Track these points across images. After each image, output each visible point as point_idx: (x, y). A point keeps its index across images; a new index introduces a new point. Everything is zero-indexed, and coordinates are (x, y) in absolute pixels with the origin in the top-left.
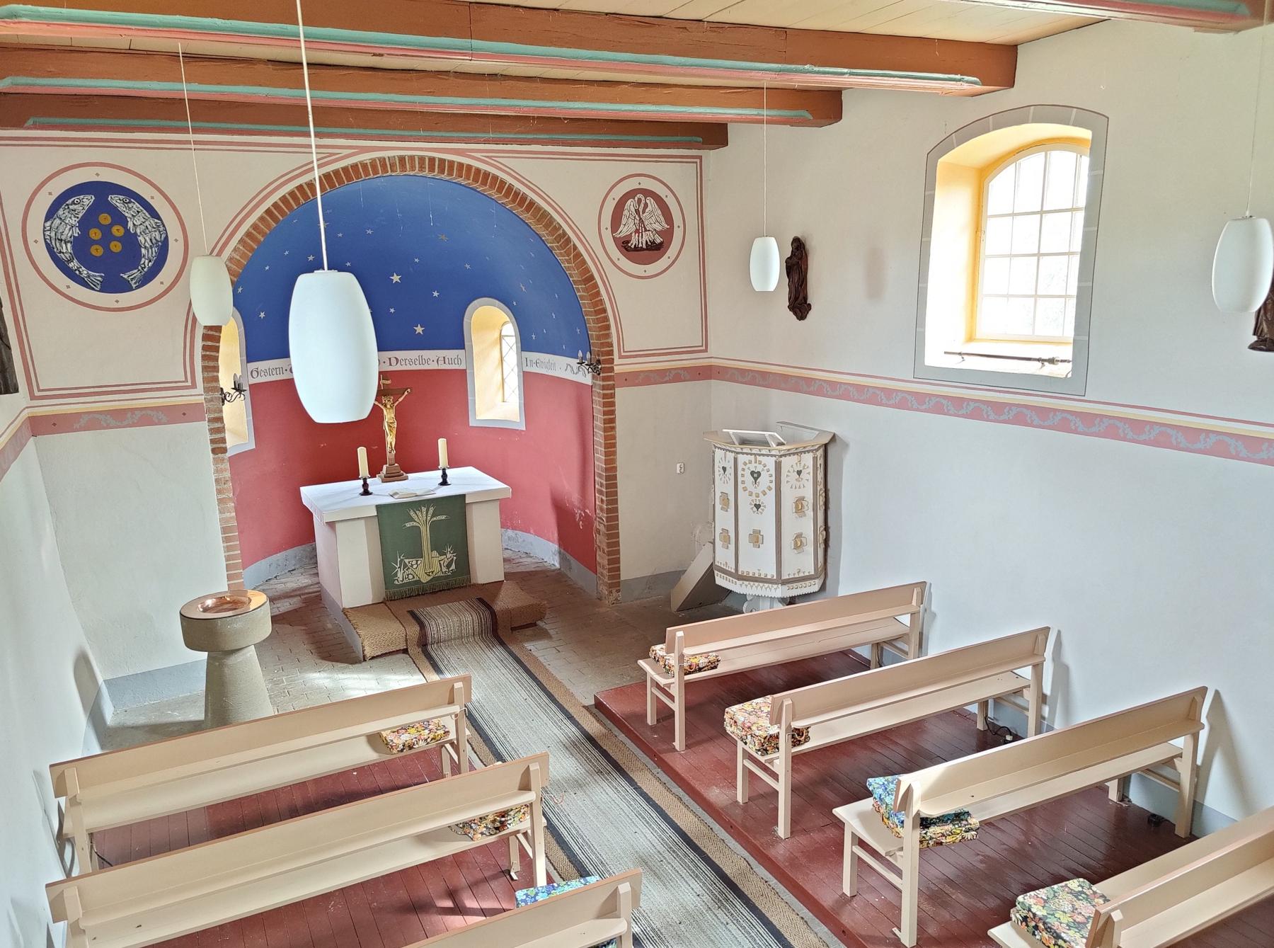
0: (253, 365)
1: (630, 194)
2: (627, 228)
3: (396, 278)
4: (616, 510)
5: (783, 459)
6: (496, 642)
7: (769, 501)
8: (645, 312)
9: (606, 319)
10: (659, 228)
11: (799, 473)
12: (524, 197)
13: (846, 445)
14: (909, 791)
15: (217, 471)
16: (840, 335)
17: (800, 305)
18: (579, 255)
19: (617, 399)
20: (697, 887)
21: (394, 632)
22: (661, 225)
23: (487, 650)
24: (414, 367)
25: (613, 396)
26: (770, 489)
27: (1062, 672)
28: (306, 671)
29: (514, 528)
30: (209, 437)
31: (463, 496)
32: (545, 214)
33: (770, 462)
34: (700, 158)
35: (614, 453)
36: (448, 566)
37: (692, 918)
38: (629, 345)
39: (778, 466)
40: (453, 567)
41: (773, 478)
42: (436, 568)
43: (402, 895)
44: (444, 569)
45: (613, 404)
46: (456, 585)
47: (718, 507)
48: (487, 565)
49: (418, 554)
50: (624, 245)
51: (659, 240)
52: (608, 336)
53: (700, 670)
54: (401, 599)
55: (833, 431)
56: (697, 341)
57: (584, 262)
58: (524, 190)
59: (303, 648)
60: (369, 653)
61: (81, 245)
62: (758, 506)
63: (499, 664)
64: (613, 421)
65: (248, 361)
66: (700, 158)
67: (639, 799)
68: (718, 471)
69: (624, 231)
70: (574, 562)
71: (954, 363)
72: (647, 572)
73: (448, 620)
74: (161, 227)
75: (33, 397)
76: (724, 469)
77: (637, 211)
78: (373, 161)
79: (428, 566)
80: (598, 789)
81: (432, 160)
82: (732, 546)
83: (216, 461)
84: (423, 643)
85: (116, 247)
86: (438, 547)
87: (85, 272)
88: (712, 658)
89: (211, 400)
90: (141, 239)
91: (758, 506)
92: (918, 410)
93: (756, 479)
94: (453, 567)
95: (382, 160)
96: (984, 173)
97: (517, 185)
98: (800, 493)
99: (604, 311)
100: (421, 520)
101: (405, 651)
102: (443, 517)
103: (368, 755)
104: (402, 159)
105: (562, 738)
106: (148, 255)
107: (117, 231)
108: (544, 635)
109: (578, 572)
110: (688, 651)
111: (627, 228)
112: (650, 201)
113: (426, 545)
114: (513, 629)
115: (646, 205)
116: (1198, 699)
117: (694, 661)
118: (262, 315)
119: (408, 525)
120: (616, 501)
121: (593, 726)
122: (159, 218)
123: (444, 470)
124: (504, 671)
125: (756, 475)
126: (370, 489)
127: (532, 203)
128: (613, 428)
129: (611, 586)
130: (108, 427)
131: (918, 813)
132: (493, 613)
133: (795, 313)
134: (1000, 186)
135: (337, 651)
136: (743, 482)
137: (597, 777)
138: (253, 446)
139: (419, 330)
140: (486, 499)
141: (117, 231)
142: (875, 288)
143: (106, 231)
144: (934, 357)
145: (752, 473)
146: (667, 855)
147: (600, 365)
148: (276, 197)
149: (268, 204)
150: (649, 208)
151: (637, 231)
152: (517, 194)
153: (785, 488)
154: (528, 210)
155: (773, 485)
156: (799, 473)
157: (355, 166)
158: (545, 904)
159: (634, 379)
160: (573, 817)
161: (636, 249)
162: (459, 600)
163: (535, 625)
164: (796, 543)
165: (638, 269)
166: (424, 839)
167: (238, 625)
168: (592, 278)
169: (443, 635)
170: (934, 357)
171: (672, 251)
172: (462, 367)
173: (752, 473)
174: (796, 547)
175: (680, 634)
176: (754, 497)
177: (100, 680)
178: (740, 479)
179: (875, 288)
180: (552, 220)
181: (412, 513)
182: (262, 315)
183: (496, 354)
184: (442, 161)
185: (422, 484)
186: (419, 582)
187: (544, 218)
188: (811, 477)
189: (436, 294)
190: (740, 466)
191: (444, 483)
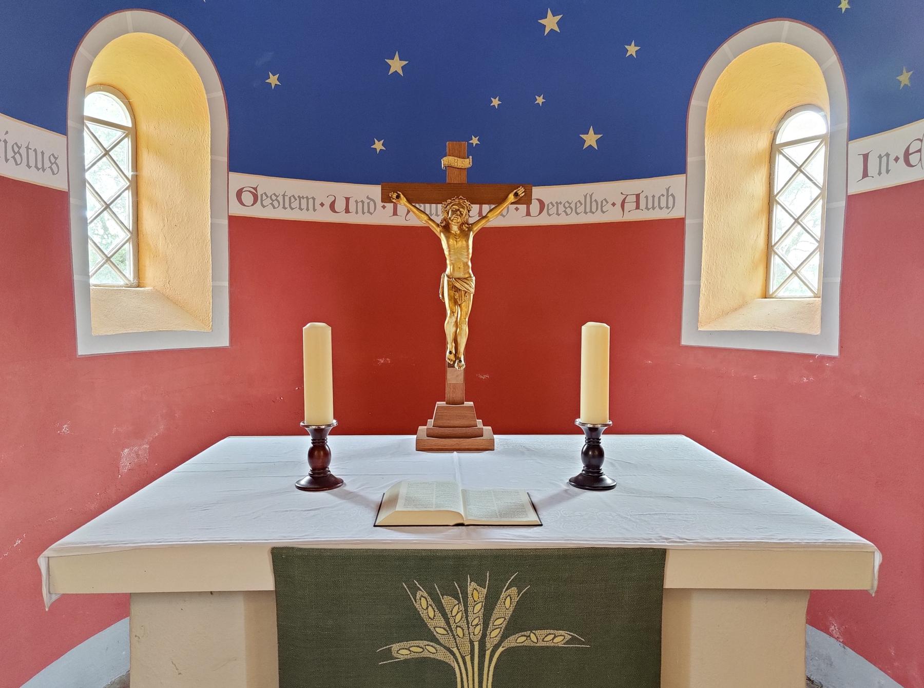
31: (653, 560)
102: (559, 638)
119: (403, 651)
123: (593, 434)
126: (334, 469)
138: (223, 341)
172: (676, 213)
183: (757, 185)
191: (591, 479)
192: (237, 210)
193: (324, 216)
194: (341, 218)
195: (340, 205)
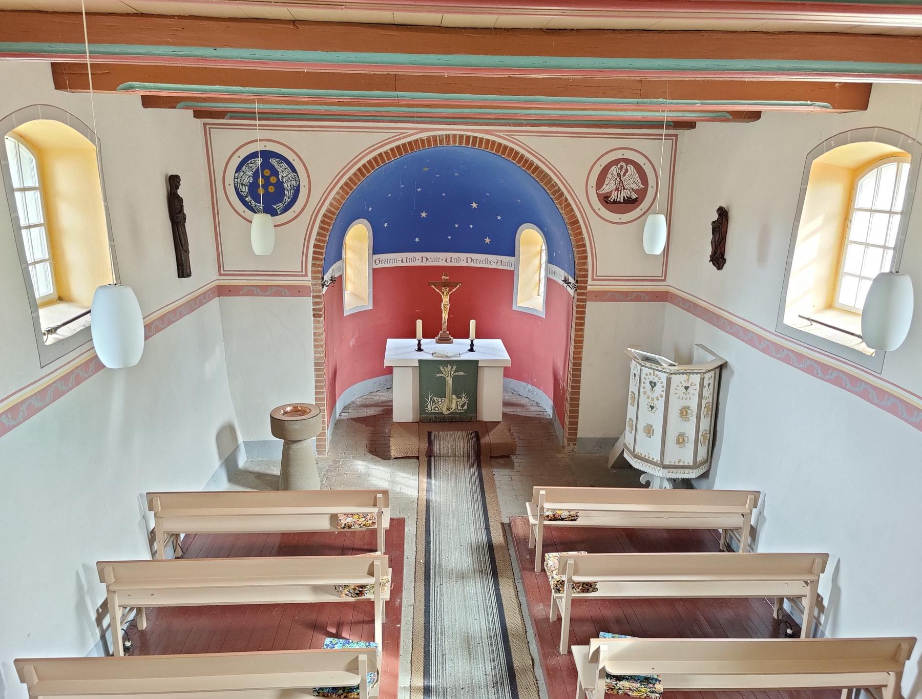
0: (376, 257)
1: (615, 162)
2: (609, 186)
5: (673, 376)
6: (475, 464)
9: (585, 252)
10: (635, 187)
11: (687, 388)
12: (532, 164)
13: (733, 372)
14: (597, 651)
15: (315, 328)
16: (735, 290)
17: (718, 259)
18: (569, 205)
19: (587, 310)
20: (489, 667)
21: (413, 444)
23: (466, 464)
25: (584, 307)
26: (662, 396)
27: (836, 591)
28: (354, 457)
29: (532, 384)
30: (312, 307)
31: (477, 361)
32: (546, 175)
33: (664, 377)
34: (676, 136)
35: (581, 347)
36: (463, 406)
37: (472, 688)
39: (669, 380)
40: (466, 407)
42: (454, 406)
43: (313, 617)
45: (584, 313)
46: (467, 420)
47: (630, 401)
48: (491, 408)
49: (443, 395)
50: (605, 200)
51: (634, 196)
52: (585, 264)
53: (562, 519)
54: (429, 424)
55: (727, 359)
56: (658, 272)
57: (572, 210)
58: (531, 158)
59: (364, 442)
60: (393, 454)
61: (253, 187)
62: (652, 407)
63: (467, 480)
64: (583, 324)
65: (374, 254)
66: (676, 136)
67: (493, 597)
68: (632, 375)
69: (606, 189)
70: (557, 419)
71: (803, 326)
72: (598, 435)
73: (452, 442)
74: (297, 179)
75: (220, 274)
77: (619, 175)
78: (428, 138)
80: (472, 583)
81: (468, 137)
82: (633, 432)
83: (315, 322)
84: (429, 456)
85: (271, 189)
86: (457, 393)
87: (254, 203)
88: (573, 513)
89: (315, 285)
91: (652, 407)
92: (774, 357)
93: (653, 387)
94: (466, 407)
95: (435, 137)
96: (857, 172)
97: (527, 155)
98: (686, 403)
99: (584, 245)
100: (448, 373)
101: (417, 458)
103: (323, 525)
104: (448, 136)
105: (474, 541)
106: (288, 194)
107: (273, 180)
108: (510, 465)
109: (557, 424)
110: (547, 506)
111: (609, 186)
112: (631, 169)
113: (449, 390)
114: (491, 457)
115: (627, 171)
116: (905, 647)
117: (559, 512)
118: (386, 225)
120: (579, 382)
121: (498, 537)
124: (468, 486)
125: (653, 384)
127: (537, 168)
128: (582, 330)
129: (569, 440)
130: (258, 295)
131: (604, 668)
132: (479, 445)
134: (867, 184)
135: (379, 450)
136: (644, 388)
137: (477, 575)
138: (371, 307)
139: (487, 240)
140: (494, 365)
142: (762, 258)
144: (791, 319)
145: (651, 382)
146: (485, 640)
147: (580, 282)
148: (364, 161)
149: (360, 165)
150: (629, 172)
151: (617, 189)
152: (526, 161)
153: (672, 398)
154: (533, 172)
155: (664, 394)
157: (416, 141)
158: (338, 651)
159: (601, 296)
160: (445, 598)
161: (615, 202)
163: (508, 457)
165: (615, 217)
166: (316, 589)
167: (297, 427)
168: (577, 221)
169: (443, 452)
170: (791, 319)
171: (644, 205)
172: (512, 269)
173: (651, 382)
174: (678, 442)
175: (543, 492)
177: (241, 440)
178: (642, 385)
179: (762, 258)
180: (550, 179)
182: (386, 225)
185: (457, 349)
186: (442, 413)
189: (499, 218)
190: (643, 376)
191: (471, 350)
192: (375, 266)
193: (400, 264)
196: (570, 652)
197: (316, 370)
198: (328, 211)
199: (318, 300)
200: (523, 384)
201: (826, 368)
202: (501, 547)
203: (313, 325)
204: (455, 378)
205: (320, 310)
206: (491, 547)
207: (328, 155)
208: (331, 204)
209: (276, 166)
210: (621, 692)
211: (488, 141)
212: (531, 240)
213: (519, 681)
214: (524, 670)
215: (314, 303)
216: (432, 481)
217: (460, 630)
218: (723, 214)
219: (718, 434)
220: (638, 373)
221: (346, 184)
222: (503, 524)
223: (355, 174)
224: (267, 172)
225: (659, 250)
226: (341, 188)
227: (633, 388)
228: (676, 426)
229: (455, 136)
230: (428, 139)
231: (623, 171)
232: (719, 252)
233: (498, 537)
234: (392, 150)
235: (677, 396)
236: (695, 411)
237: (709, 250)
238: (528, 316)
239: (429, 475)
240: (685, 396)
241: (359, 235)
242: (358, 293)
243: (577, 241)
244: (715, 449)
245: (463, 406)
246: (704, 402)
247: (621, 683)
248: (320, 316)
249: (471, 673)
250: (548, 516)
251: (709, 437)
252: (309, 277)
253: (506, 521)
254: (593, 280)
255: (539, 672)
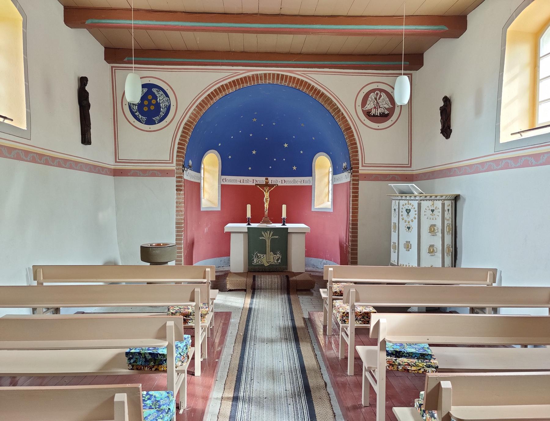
3: (286, 145)
4: (356, 241)
5: (422, 202)
7: (414, 225)
8: (376, 146)
10: (387, 107)
12: (319, 91)
13: (464, 200)
15: (177, 198)
19: (360, 186)
20: (289, 387)
22: (389, 105)
23: (279, 293)
24: (291, 184)
25: (358, 184)
26: (415, 218)
30: (175, 184)
32: (329, 99)
33: (415, 204)
34: (411, 74)
36: (278, 260)
38: (368, 161)
39: (419, 205)
40: (280, 261)
41: (417, 212)
42: (272, 260)
44: (275, 261)
45: (358, 188)
46: (281, 268)
47: (392, 230)
49: (264, 252)
50: (368, 114)
51: (386, 112)
52: (357, 156)
54: (254, 270)
57: (347, 121)
58: (319, 88)
60: (229, 287)
62: (409, 228)
64: (357, 197)
65: (222, 175)
66: (411, 74)
68: (393, 211)
69: (368, 107)
74: (169, 100)
75: (116, 162)
76: (395, 210)
77: (376, 99)
78: (253, 75)
79: (269, 259)
81: (278, 75)
83: (177, 194)
86: (274, 251)
87: (140, 116)
89: (178, 169)
90: (161, 105)
91: (409, 228)
93: (408, 213)
94: (280, 261)
95: (257, 75)
97: (316, 86)
98: (433, 222)
100: (267, 237)
101: (245, 290)
104: (265, 74)
107: (154, 102)
112: (383, 95)
113: (268, 249)
115: (381, 96)
118: (230, 157)
119: (261, 238)
122: (168, 97)
125: (408, 211)
127: (323, 94)
128: (357, 200)
133: (444, 135)
137: (290, 401)
138: (219, 209)
139: (295, 168)
141: (154, 102)
142: (478, 111)
143: (150, 101)
145: (407, 210)
151: (375, 108)
152: (316, 89)
153: (423, 218)
155: (417, 216)
156: (433, 211)
157: (245, 78)
161: (374, 116)
162: (307, 297)
164: (429, 249)
165: (375, 125)
168: (350, 128)
171: (394, 118)
172: (311, 184)
173: (407, 210)
176: (407, 223)
178: (401, 214)
179: (478, 111)
180: (332, 101)
181: (263, 233)
182: (230, 157)
184: (283, 75)
186: (263, 265)
187: (328, 100)
188: (440, 214)
190: (401, 206)
192: (223, 183)
193: (239, 183)
194: (242, 184)
195: (242, 181)
196: (356, 351)
197: (177, 227)
198: (188, 121)
199: (180, 179)
200: (321, 260)
201: (536, 156)
202: (302, 328)
203: (175, 197)
204: (273, 241)
205: (181, 186)
206: (294, 328)
207: (189, 87)
208: (190, 117)
209: (156, 93)
210: (400, 368)
211: (291, 77)
212: (322, 163)
213: (313, 395)
214: (318, 388)
215: (177, 182)
216: (254, 300)
217: (267, 367)
218: (447, 101)
219: (458, 250)
220: (397, 208)
221: (200, 104)
222: (304, 319)
223: (206, 98)
224: (150, 97)
225: (406, 101)
226: (197, 106)
227: (394, 220)
228: (427, 240)
229: (269, 74)
230: (253, 76)
231: (378, 96)
232: (446, 126)
233: (299, 323)
234: (230, 83)
235: (426, 217)
236: (440, 228)
237: (440, 126)
238: (323, 213)
239: (252, 297)
240: (432, 217)
241: (211, 161)
242: (210, 197)
243: (351, 141)
244: (457, 261)
245: (278, 260)
246: (446, 222)
247: (400, 359)
248: (181, 190)
249: (274, 389)
250: (336, 292)
251: (452, 249)
252: (174, 164)
253: (306, 316)
254: (363, 166)
255: (330, 390)
